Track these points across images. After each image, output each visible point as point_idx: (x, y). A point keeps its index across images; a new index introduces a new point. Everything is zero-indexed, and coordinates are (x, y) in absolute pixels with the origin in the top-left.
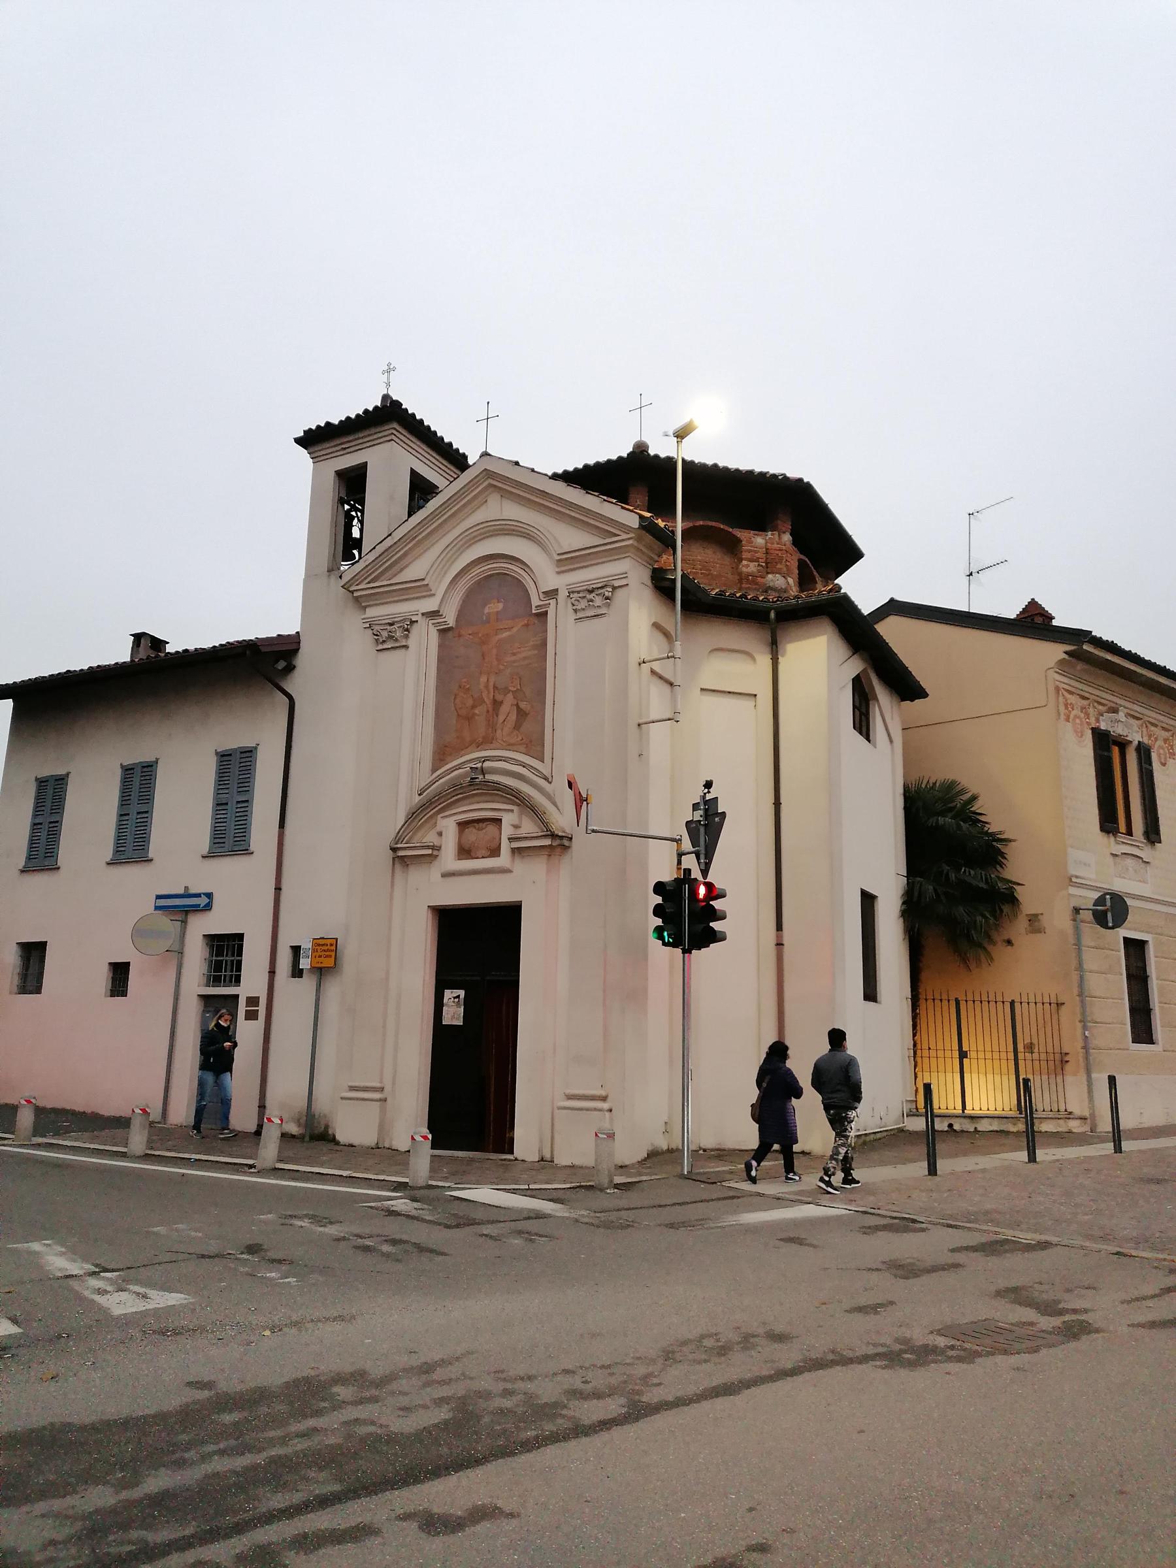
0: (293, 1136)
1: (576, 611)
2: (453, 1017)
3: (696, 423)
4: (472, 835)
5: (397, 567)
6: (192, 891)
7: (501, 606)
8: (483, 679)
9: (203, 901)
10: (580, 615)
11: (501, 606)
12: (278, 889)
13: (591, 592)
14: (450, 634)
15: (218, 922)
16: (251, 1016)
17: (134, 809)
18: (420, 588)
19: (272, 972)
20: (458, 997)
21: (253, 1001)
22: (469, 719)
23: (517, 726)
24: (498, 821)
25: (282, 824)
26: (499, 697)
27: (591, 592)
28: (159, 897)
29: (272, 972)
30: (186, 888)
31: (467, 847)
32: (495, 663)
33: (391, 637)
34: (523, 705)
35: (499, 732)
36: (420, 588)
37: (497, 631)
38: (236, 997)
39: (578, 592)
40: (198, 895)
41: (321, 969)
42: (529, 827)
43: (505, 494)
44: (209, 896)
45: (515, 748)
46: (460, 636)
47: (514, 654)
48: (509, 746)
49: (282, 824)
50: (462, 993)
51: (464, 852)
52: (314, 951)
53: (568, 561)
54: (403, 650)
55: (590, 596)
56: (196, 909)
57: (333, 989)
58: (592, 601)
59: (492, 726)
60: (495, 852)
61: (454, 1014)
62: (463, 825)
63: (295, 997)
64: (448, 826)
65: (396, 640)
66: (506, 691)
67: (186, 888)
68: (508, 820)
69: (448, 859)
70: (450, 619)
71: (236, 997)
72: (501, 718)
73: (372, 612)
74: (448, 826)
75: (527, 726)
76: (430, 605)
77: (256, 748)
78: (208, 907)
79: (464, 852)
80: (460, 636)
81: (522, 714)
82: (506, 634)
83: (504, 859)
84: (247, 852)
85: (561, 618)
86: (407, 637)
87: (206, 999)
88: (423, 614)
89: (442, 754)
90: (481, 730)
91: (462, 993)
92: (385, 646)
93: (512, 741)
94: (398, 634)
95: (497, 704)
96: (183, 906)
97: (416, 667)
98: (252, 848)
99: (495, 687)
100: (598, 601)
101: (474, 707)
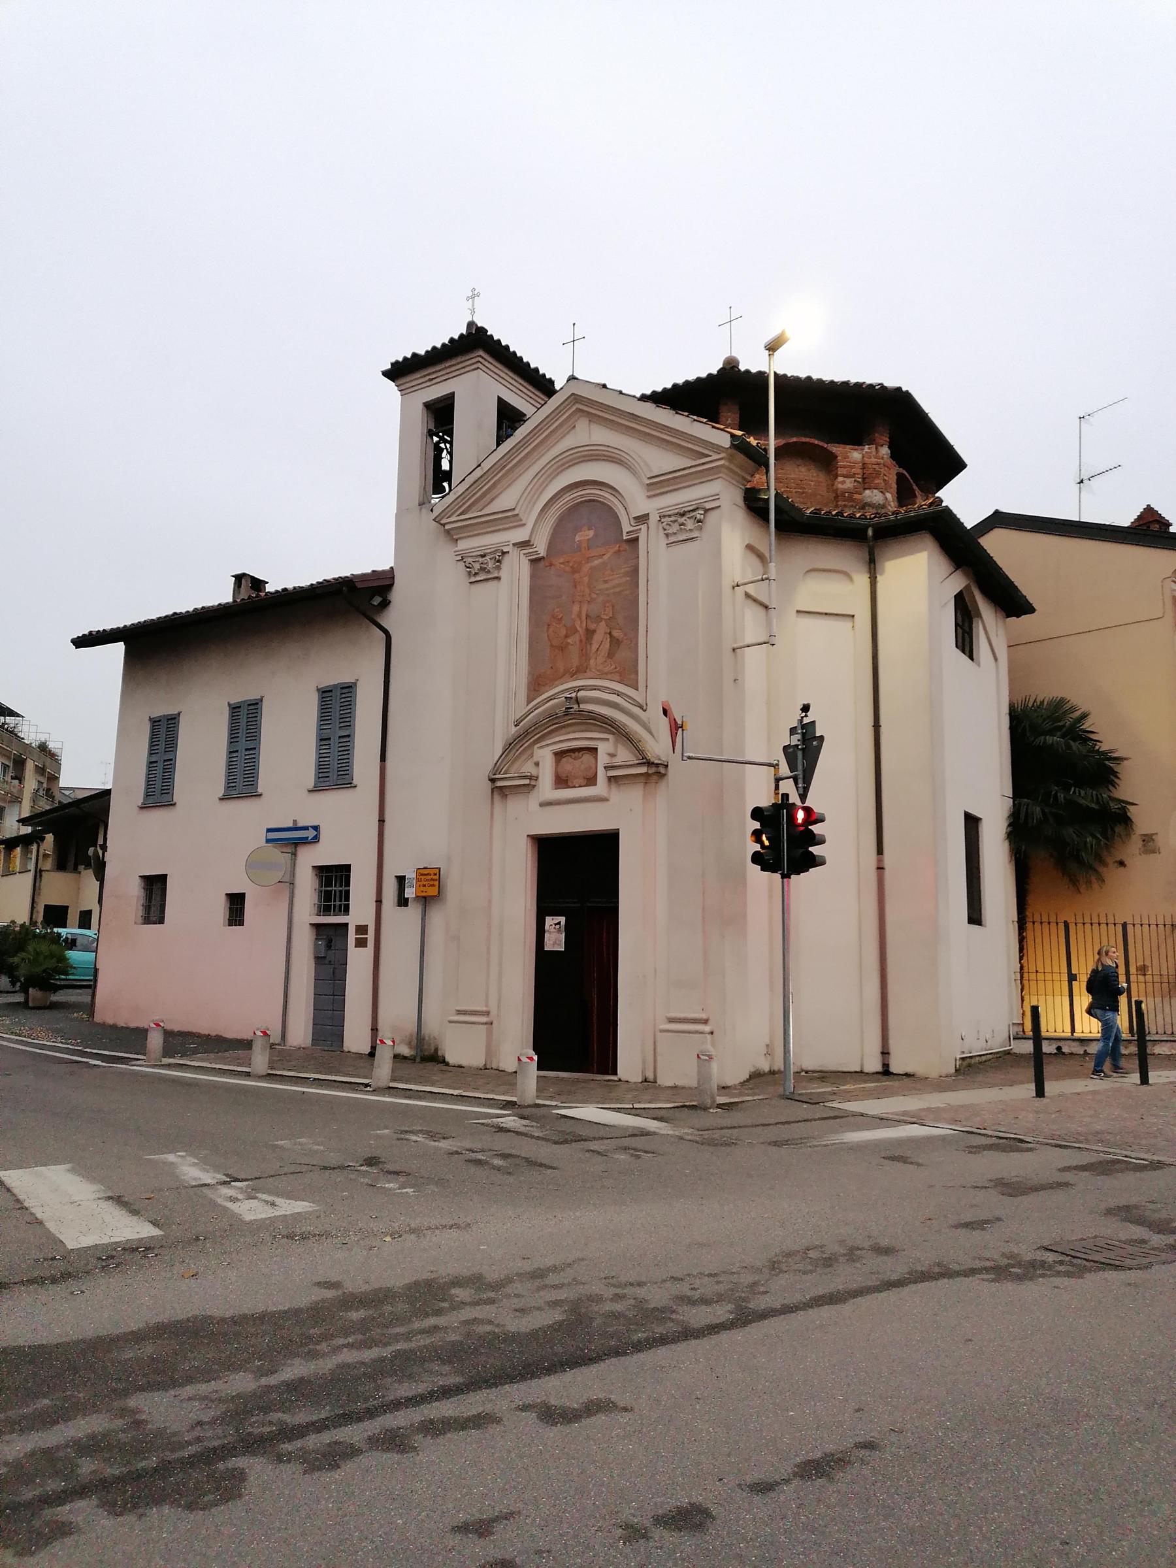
0: (405, 1058)
1: (667, 535)
2: (554, 943)
3: (788, 334)
4: (568, 765)
5: (482, 503)
6: (300, 824)
7: (577, 538)
8: (576, 608)
9: (311, 834)
10: (672, 539)
11: (591, 533)
12: (382, 821)
13: (682, 515)
14: (542, 564)
15: (326, 854)
16: (361, 943)
17: (242, 745)
18: (510, 519)
19: (379, 902)
20: (559, 923)
21: (362, 929)
22: (562, 648)
23: (611, 655)
24: (594, 750)
25: (383, 758)
26: (592, 626)
27: (682, 515)
28: (269, 830)
29: (379, 902)
30: (295, 822)
31: (563, 776)
32: (587, 591)
33: (483, 569)
34: (615, 633)
35: (592, 662)
36: (510, 519)
37: (589, 559)
38: (346, 925)
39: (670, 516)
40: (306, 828)
41: (425, 897)
42: (624, 755)
43: (593, 418)
44: (316, 828)
45: (609, 676)
46: (551, 565)
47: (606, 582)
48: (603, 675)
49: (383, 758)
50: (563, 920)
51: (561, 781)
52: (418, 880)
53: (659, 485)
54: (495, 582)
55: (682, 520)
56: (305, 842)
57: (437, 917)
58: (683, 524)
59: (584, 654)
60: (591, 781)
61: (555, 941)
62: (559, 755)
63: (401, 926)
64: (545, 755)
65: (489, 572)
66: (598, 619)
67: (295, 822)
68: (603, 749)
69: (546, 789)
70: (541, 549)
71: (346, 925)
72: (595, 647)
73: (463, 545)
74: (545, 755)
75: (622, 654)
76: (521, 535)
77: (355, 684)
78: (316, 839)
79: (561, 781)
80: (551, 565)
81: (615, 642)
82: (596, 562)
83: (601, 788)
84: (350, 785)
85: (653, 543)
86: (499, 568)
87: (318, 927)
88: (514, 545)
89: (537, 684)
90: (575, 661)
91: (563, 920)
92: (478, 578)
93: (606, 670)
94: (491, 565)
95: (590, 633)
96: (293, 839)
97: (509, 597)
98: (355, 782)
99: (587, 616)
100: (690, 524)
101: (566, 636)
